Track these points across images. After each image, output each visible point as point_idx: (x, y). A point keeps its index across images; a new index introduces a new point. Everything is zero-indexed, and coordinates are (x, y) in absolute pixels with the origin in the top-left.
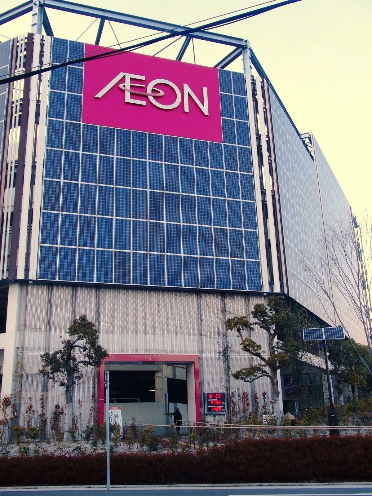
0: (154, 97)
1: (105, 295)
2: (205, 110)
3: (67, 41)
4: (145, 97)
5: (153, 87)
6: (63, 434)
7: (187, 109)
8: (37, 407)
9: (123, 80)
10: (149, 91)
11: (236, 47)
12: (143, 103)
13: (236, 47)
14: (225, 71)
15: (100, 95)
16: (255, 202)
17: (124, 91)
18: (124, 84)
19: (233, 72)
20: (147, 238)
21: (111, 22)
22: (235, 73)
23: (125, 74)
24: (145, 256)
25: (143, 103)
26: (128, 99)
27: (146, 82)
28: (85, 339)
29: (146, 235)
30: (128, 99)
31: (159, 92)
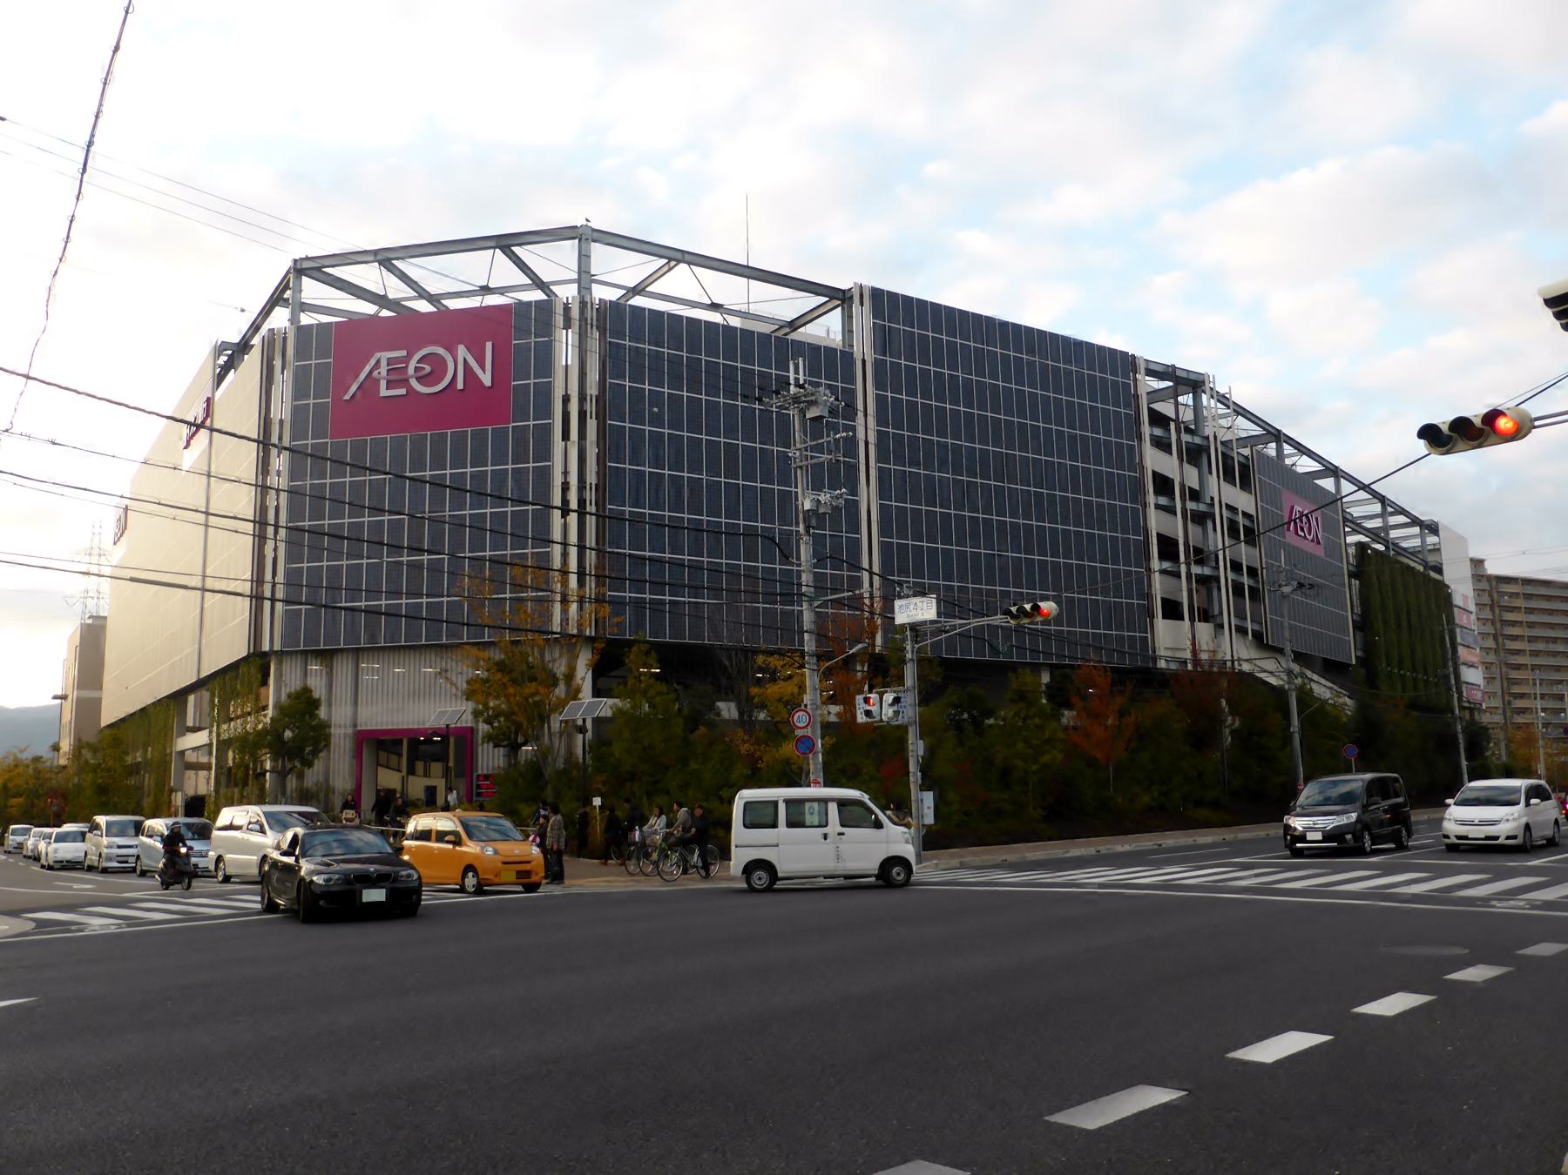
2: (486, 379)
3: (754, 332)
4: (404, 382)
5: (417, 363)
7: (460, 386)
8: (449, 661)
10: (411, 371)
11: (513, 248)
12: (402, 391)
16: (859, 536)
17: (379, 380)
19: (649, 309)
25: (402, 391)
26: (384, 392)
30: (384, 392)
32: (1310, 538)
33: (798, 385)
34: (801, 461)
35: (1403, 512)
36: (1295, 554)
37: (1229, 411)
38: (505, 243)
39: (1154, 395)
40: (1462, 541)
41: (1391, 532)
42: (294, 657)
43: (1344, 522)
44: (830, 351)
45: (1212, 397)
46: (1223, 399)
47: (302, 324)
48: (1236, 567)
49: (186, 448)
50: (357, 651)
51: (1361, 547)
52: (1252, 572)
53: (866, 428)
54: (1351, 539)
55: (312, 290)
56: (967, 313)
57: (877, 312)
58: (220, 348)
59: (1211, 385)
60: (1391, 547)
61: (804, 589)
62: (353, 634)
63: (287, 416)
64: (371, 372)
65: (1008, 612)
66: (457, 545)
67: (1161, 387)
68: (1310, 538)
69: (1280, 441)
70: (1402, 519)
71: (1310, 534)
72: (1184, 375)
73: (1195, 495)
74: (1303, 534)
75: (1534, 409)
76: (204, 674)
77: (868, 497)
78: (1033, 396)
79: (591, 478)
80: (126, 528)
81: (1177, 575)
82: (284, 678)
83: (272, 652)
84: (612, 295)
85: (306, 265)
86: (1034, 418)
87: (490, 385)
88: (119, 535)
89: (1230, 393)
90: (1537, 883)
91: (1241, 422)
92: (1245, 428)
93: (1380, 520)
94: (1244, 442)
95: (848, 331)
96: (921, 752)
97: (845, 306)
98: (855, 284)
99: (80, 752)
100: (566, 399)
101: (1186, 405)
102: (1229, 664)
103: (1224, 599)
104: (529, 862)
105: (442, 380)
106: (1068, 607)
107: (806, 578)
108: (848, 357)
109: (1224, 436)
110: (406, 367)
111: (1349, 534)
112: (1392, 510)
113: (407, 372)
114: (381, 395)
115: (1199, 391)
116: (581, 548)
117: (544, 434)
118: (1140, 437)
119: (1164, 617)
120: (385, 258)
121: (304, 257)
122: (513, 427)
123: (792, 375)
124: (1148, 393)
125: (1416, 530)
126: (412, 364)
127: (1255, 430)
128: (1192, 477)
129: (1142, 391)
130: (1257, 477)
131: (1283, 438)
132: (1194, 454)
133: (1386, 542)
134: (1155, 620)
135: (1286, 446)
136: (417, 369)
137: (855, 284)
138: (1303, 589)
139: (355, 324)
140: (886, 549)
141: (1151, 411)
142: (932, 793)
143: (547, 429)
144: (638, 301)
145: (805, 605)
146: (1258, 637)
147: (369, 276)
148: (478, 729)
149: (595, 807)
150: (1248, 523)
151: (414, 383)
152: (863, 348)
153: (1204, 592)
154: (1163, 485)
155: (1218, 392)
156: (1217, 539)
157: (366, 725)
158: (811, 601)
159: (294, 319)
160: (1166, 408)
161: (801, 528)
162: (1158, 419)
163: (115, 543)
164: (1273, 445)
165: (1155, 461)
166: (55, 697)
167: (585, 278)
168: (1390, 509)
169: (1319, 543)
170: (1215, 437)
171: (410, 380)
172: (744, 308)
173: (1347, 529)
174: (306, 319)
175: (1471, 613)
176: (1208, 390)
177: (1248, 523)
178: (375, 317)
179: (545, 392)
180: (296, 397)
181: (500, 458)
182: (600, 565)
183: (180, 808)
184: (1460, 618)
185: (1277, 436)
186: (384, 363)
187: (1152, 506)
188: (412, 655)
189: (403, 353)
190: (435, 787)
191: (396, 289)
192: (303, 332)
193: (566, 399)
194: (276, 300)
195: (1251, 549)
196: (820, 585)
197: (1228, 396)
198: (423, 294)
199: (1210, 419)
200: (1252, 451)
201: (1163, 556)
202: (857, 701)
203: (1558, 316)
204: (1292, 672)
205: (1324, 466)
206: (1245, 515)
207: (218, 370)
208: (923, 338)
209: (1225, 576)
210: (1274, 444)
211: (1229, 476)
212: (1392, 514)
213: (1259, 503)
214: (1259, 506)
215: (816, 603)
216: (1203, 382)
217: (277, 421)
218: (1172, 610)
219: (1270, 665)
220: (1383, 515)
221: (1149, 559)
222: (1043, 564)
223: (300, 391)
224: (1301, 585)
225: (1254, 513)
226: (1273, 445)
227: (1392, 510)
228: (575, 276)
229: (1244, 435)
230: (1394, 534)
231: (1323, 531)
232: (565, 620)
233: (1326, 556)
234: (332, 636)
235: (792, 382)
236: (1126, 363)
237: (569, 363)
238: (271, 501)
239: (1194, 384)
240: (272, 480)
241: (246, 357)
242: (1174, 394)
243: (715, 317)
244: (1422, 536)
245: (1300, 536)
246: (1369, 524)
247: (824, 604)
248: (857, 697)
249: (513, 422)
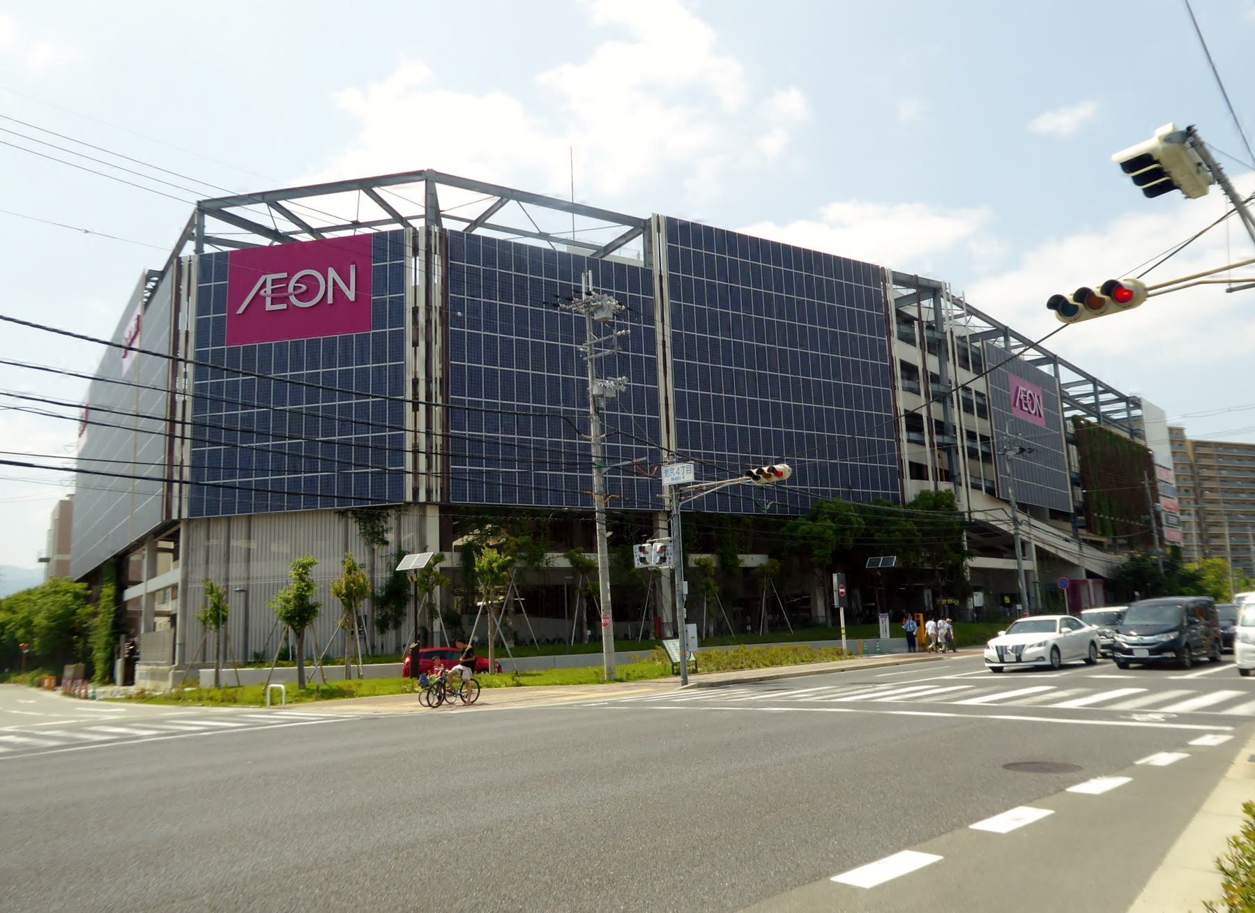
2: (351, 295)
4: (285, 300)
6: (618, 344)
7: (330, 300)
9: (264, 285)
10: (291, 289)
12: (284, 306)
13: (632, 228)
14: (473, 235)
15: (240, 311)
19: (483, 237)
21: (273, 227)
22: (486, 237)
25: (284, 306)
26: (269, 307)
27: (287, 280)
30: (269, 307)
31: (301, 287)
32: (1033, 412)
33: (589, 294)
34: (591, 354)
35: (1108, 390)
36: (1019, 426)
37: (963, 312)
38: (367, 185)
39: (900, 301)
40: (1161, 415)
41: (1102, 407)
42: (294, 517)
43: (1061, 400)
44: (633, 269)
45: (948, 300)
46: (958, 302)
47: (205, 253)
48: (971, 436)
51: (1075, 419)
52: (984, 439)
53: (663, 331)
54: (1068, 414)
55: (213, 226)
56: (819, 254)
57: (671, 237)
58: (148, 276)
59: (948, 291)
60: (1101, 418)
61: (594, 459)
63: (192, 330)
65: (750, 474)
66: (312, 430)
67: (909, 293)
68: (1033, 412)
69: (1007, 336)
70: (1111, 396)
71: (1033, 409)
72: (925, 283)
73: (935, 379)
74: (1026, 409)
75: (1148, 281)
77: (666, 386)
78: (821, 306)
79: (437, 372)
81: (922, 443)
84: (460, 227)
85: (207, 205)
86: (802, 320)
87: (354, 300)
89: (964, 297)
90: (1193, 694)
91: (974, 320)
92: (979, 325)
93: (1093, 397)
94: (975, 337)
95: (649, 252)
96: (686, 592)
97: (646, 232)
98: (653, 214)
100: (415, 311)
101: (929, 308)
102: (967, 516)
103: (962, 463)
104: (1024, 555)
105: (314, 297)
106: (799, 474)
107: (595, 451)
108: (647, 273)
109: (958, 332)
110: (287, 286)
111: (1067, 409)
112: (1102, 389)
113: (287, 291)
114: (267, 309)
115: (938, 296)
116: (429, 434)
117: (399, 338)
118: (889, 334)
119: (912, 478)
120: (272, 199)
123: (583, 285)
124: (895, 300)
125: (1123, 405)
126: (292, 283)
127: (987, 327)
128: (933, 364)
129: (891, 298)
130: (988, 365)
131: (1009, 332)
132: (936, 346)
133: (1098, 415)
134: (904, 480)
135: (1012, 339)
136: (295, 288)
137: (653, 214)
138: (1025, 453)
139: (248, 251)
140: (681, 427)
141: (899, 313)
142: (695, 625)
143: (401, 336)
144: (479, 231)
145: (594, 471)
146: (991, 492)
147: (259, 214)
150: (980, 401)
151: (293, 300)
152: (660, 266)
153: (945, 455)
154: (909, 370)
155: (953, 297)
156: (958, 417)
158: (599, 468)
159: (199, 250)
160: (912, 311)
161: (591, 410)
162: (906, 320)
164: (1002, 339)
165: (902, 352)
166: (41, 560)
167: (433, 212)
168: (1100, 389)
169: (1040, 416)
170: (952, 332)
171: (290, 297)
172: (570, 236)
173: (1065, 405)
174: (208, 249)
175: (1169, 470)
176: (945, 296)
177: (980, 401)
178: (271, 247)
179: (399, 304)
180: (199, 312)
181: (346, 361)
182: (445, 445)
184: (1160, 474)
185: (1005, 332)
186: (269, 283)
187: (900, 388)
188: (328, 518)
189: (284, 275)
191: (285, 226)
192: (204, 260)
193: (415, 311)
194: (186, 236)
195: (982, 421)
196: (611, 455)
197: (962, 299)
198: (306, 228)
199: (947, 319)
200: (983, 344)
201: (910, 428)
202: (634, 551)
203: (1138, 180)
204: (1016, 520)
205: (1045, 355)
206: (978, 394)
208: (710, 258)
209: (962, 443)
210: (1003, 338)
211: (964, 363)
212: (1102, 392)
213: (989, 385)
214: (989, 387)
215: (605, 470)
216: (941, 288)
217: (184, 332)
218: (918, 471)
219: (1000, 515)
220: (1095, 393)
221: (899, 431)
222: (789, 435)
223: (202, 308)
224: (1022, 450)
225: (985, 393)
226: (1002, 339)
227: (1102, 389)
228: (423, 212)
229: (978, 331)
230: (1103, 409)
231: (1044, 406)
233: (1047, 426)
235: (584, 290)
236: (872, 274)
237: (418, 284)
238: (179, 398)
239: (932, 290)
240: (181, 384)
242: (917, 298)
243: (543, 244)
244: (1128, 410)
245: (1025, 411)
246: (1086, 401)
247: (615, 470)
248: (634, 546)
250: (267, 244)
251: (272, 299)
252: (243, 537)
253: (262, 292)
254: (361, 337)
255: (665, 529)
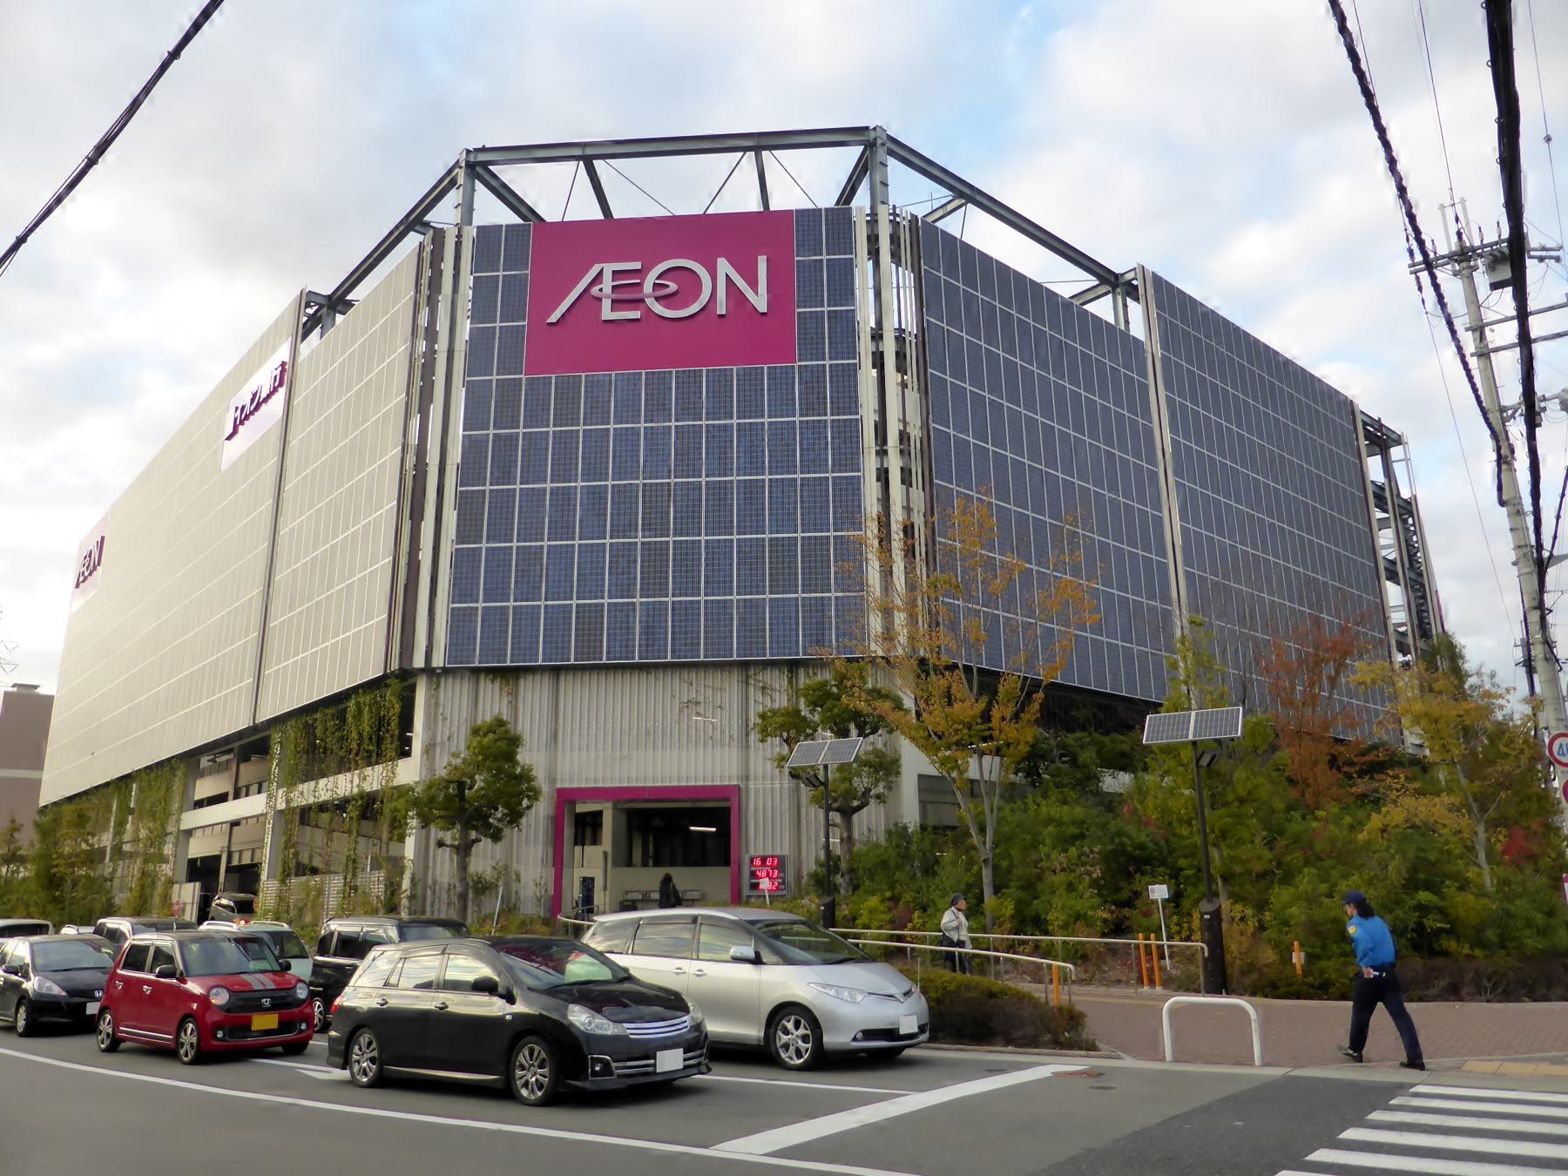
0: (657, 299)
1: (567, 684)
2: (760, 302)
4: (638, 302)
7: (721, 310)
9: (598, 278)
10: (648, 287)
12: (636, 314)
17: (600, 299)
18: (599, 287)
20: (635, 573)
23: (603, 265)
24: (824, 482)
25: (636, 314)
26: (607, 313)
28: (1519, 722)
29: (636, 568)
30: (607, 313)
31: (667, 286)
42: (458, 681)
49: (227, 439)
50: (556, 671)
62: (556, 640)
64: (586, 290)
76: (261, 719)
80: (99, 564)
82: (441, 710)
83: (428, 671)
88: (86, 574)
98: (1139, 265)
99: (12, 836)
113: (642, 291)
121: (480, 146)
122: (800, 367)
137: (1139, 265)
148: (747, 789)
149: (1155, 902)
157: (571, 780)
163: (77, 586)
183: (188, 908)
186: (607, 276)
190: (592, 879)
207: (305, 319)
232: (888, 635)
234: (525, 644)
241: (339, 318)
249: (800, 360)
250: (1066, 291)
251: (613, 301)
252: (544, 1013)
253: (595, 290)
254: (506, 383)
255: (1500, 236)
